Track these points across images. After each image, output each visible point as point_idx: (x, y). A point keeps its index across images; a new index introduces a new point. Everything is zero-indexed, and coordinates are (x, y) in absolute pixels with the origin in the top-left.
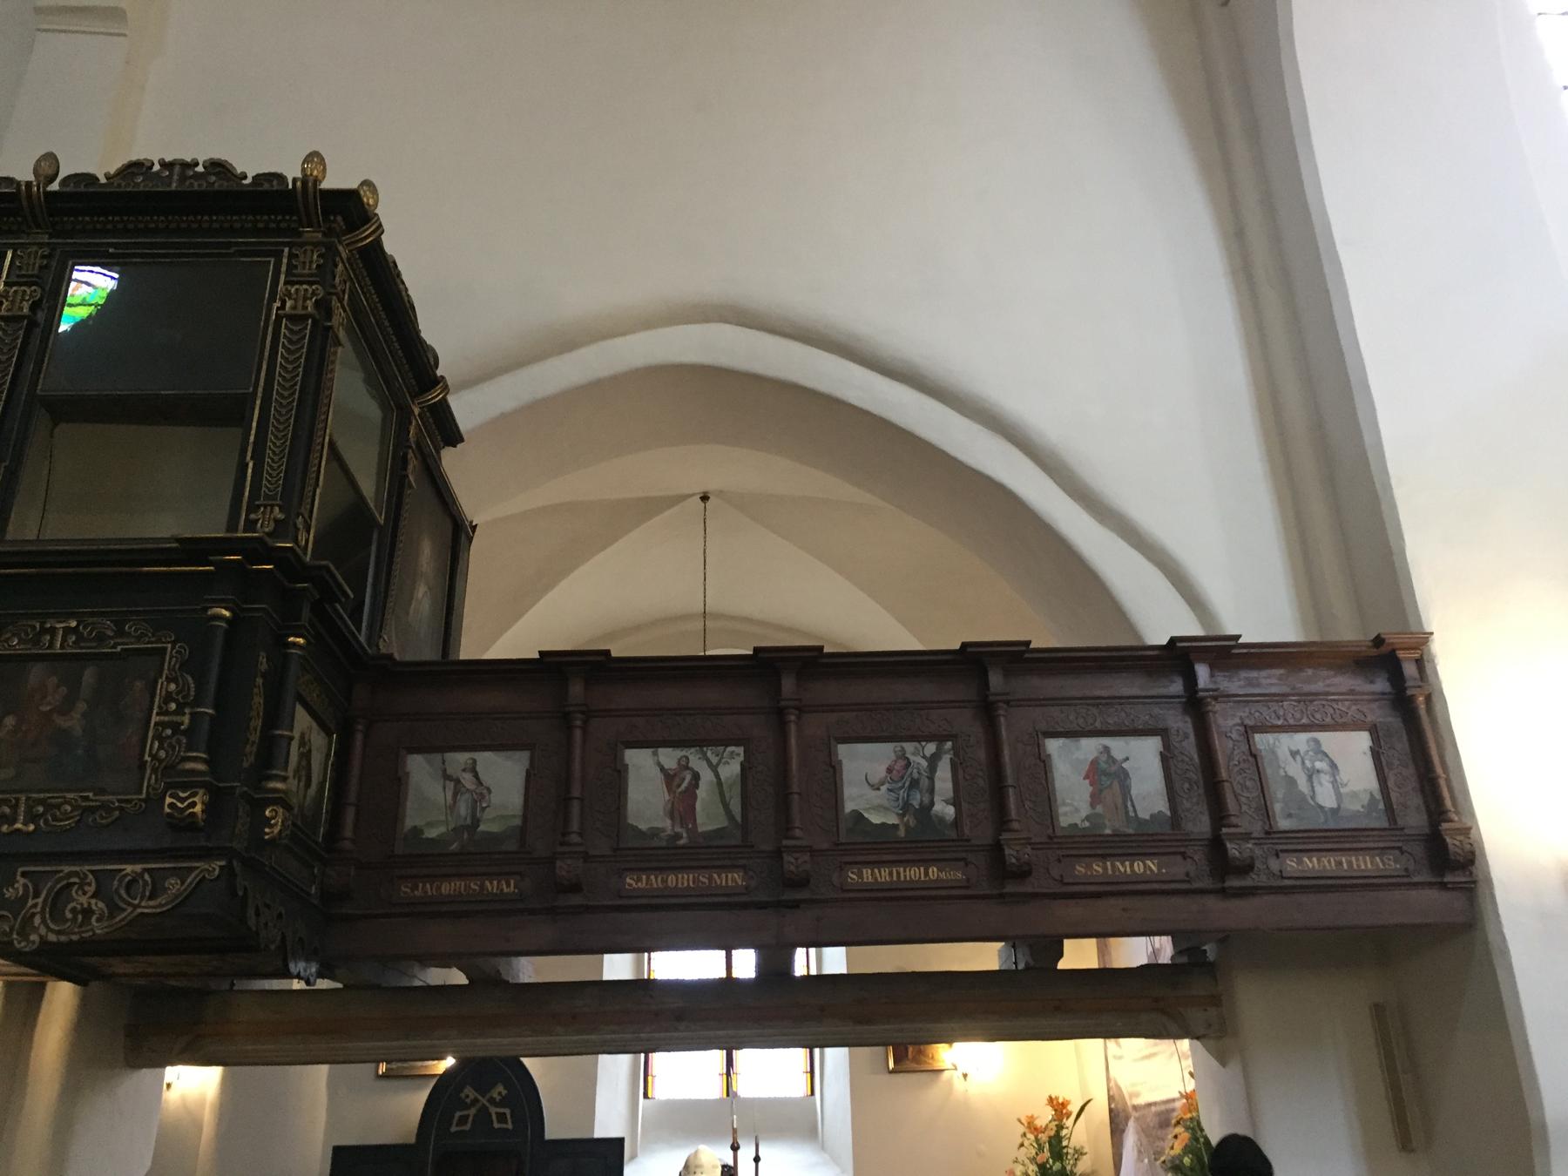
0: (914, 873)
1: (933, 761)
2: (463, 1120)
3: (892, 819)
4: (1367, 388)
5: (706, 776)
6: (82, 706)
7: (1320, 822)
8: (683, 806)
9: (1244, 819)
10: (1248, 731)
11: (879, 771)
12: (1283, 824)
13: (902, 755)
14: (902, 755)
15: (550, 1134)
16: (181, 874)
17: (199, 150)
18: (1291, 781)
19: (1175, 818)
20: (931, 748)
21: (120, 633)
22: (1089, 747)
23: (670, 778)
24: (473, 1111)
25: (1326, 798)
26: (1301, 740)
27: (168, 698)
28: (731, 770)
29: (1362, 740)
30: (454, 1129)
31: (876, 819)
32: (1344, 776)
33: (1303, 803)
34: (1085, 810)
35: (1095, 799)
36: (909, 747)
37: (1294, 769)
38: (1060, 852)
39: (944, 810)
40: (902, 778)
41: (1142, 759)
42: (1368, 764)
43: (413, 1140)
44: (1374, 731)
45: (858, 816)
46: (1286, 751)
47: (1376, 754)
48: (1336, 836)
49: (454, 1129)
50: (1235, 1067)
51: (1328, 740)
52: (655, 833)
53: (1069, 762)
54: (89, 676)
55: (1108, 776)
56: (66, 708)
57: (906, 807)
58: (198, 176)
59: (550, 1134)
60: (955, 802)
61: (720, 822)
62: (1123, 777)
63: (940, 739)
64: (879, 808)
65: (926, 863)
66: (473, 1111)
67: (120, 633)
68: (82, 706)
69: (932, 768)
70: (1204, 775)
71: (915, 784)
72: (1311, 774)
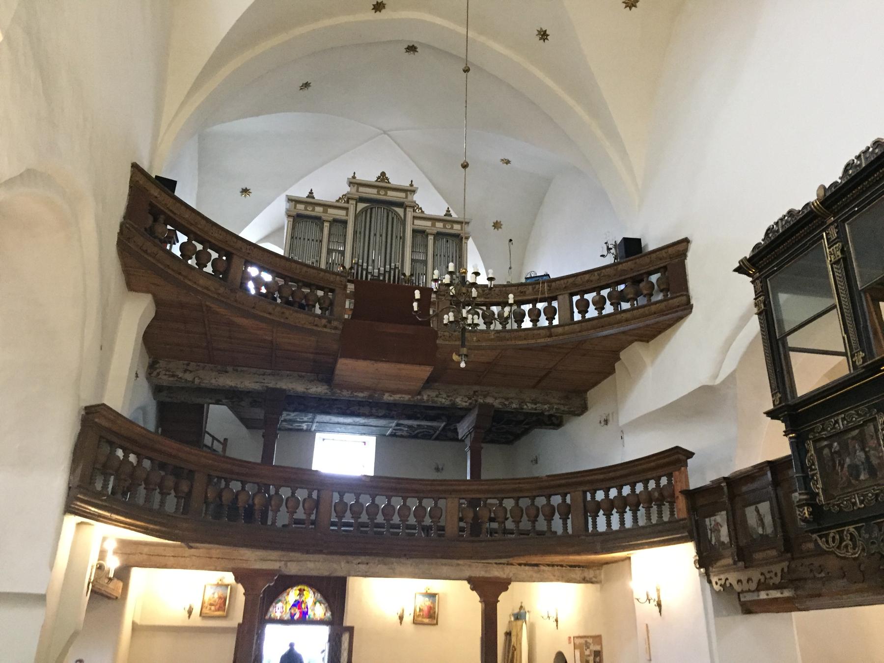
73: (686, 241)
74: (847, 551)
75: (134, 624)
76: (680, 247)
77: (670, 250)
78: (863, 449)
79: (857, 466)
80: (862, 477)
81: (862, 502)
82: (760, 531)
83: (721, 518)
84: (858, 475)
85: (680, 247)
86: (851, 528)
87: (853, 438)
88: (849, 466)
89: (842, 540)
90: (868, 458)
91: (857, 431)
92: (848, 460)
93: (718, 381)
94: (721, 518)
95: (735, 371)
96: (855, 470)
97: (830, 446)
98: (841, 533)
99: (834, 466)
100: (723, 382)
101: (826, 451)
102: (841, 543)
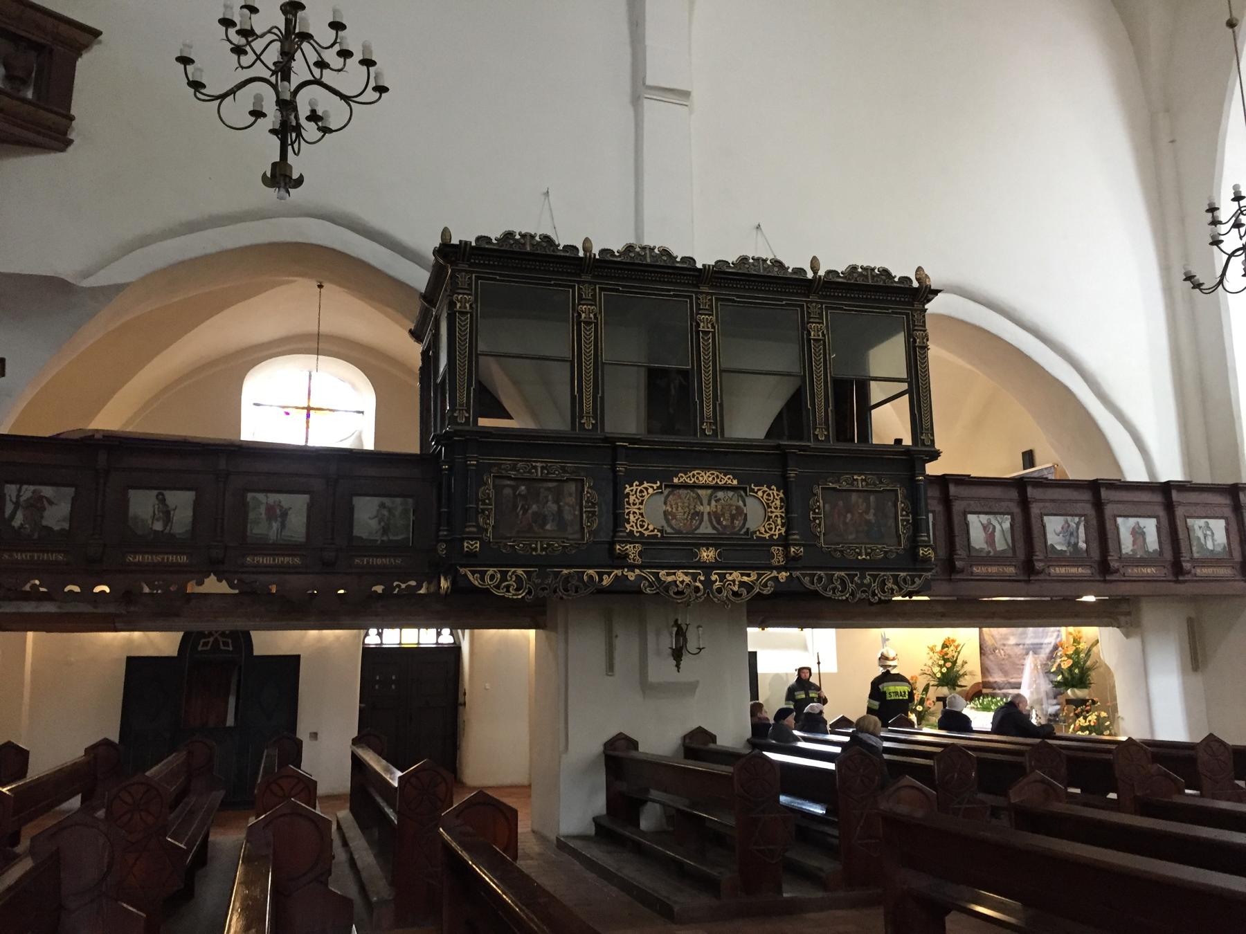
0: (1073, 570)
1: (1078, 524)
2: (205, 644)
3: (1064, 548)
4: (1235, 370)
5: (998, 527)
6: (872, 511)
7: (1209, 555)
8: (990, 539)
9: (1185, 555)
10: (1186, 517)
11: (1059, 529)
12: (1196, 555)
13: (1067, 522)
14: (1067, 522)
15: (256, 653)
16: (920, 577)
17: (877, 263)
18: (1199, 538)
19: (1161, 552)
20: (1077, 519)
21: (881, 482)
22: (1132, 522)
23: (985, 528)
24: (211, 639)
25: (1210, 546)
26: (1202, 522)
27: (903, 510)
28: (1007, 525)
29: (1222, 523)
30: (200, 648)
31: (1059, 548)
32: (1216, 537)
33: (1202, 547)
34: (1131, 547)
35: (1134, 543)
36: (1069, 518)
37: (1200, 534)
38: (467, 428)
39: (1083, 545)
40: (1069, 533)
41: (1150, 526)
42: (1224, 533)
43: (175, 654)
44: (1226, 519)
45: (1052, 546)
46: (1197, 524)
47: (1227, 530)
48: (1213, 560)
49: (200, 648)
50: (1135, 642)
51: (1212, 522)
52: (981, 550)
53: (1125, 526)
54: (872, 498)
55: (1138, 533)
56: (867, 512)
57: (1069, 544)
58: (873, 277)
59: (256, 653)
60: (1086, 542)
61: (1005, 547)
62: (1143, 534)
63: (1080, 516)
64: (1059, 543)
65: (1078, 566)
66: (211, 639)
67: (881, 482)
68: (872, 511)
69: (1078, 528)
70: (1173, 534)
71: (1072, 534)
72: (1205, 536)
73: (96, 34)
74: (508, 591)
75: (292, 662)
76: (83, 37)
77: (63, 28)
78: (557, 501)
79: (545, 517)
80: (548, 527)
81: (543, 549)
82: (158, 526)
83: (142, 504)
84: (545, 524)
85: (83, 37)
86: (520, 571)
87: (549, 489)
88: (534, 513)
89: (504, 579)
90: (560, 510)
91: (555, 484)
92: (535, 507)
93: (86, 283)
94: (142, 504)
95: (127, 284)
96: (541, 519)
97: (515, 488)
98: (504, 574)
99: (515, 507)
100: (92, 290)
101: (507, 491)
102: (501, 582)
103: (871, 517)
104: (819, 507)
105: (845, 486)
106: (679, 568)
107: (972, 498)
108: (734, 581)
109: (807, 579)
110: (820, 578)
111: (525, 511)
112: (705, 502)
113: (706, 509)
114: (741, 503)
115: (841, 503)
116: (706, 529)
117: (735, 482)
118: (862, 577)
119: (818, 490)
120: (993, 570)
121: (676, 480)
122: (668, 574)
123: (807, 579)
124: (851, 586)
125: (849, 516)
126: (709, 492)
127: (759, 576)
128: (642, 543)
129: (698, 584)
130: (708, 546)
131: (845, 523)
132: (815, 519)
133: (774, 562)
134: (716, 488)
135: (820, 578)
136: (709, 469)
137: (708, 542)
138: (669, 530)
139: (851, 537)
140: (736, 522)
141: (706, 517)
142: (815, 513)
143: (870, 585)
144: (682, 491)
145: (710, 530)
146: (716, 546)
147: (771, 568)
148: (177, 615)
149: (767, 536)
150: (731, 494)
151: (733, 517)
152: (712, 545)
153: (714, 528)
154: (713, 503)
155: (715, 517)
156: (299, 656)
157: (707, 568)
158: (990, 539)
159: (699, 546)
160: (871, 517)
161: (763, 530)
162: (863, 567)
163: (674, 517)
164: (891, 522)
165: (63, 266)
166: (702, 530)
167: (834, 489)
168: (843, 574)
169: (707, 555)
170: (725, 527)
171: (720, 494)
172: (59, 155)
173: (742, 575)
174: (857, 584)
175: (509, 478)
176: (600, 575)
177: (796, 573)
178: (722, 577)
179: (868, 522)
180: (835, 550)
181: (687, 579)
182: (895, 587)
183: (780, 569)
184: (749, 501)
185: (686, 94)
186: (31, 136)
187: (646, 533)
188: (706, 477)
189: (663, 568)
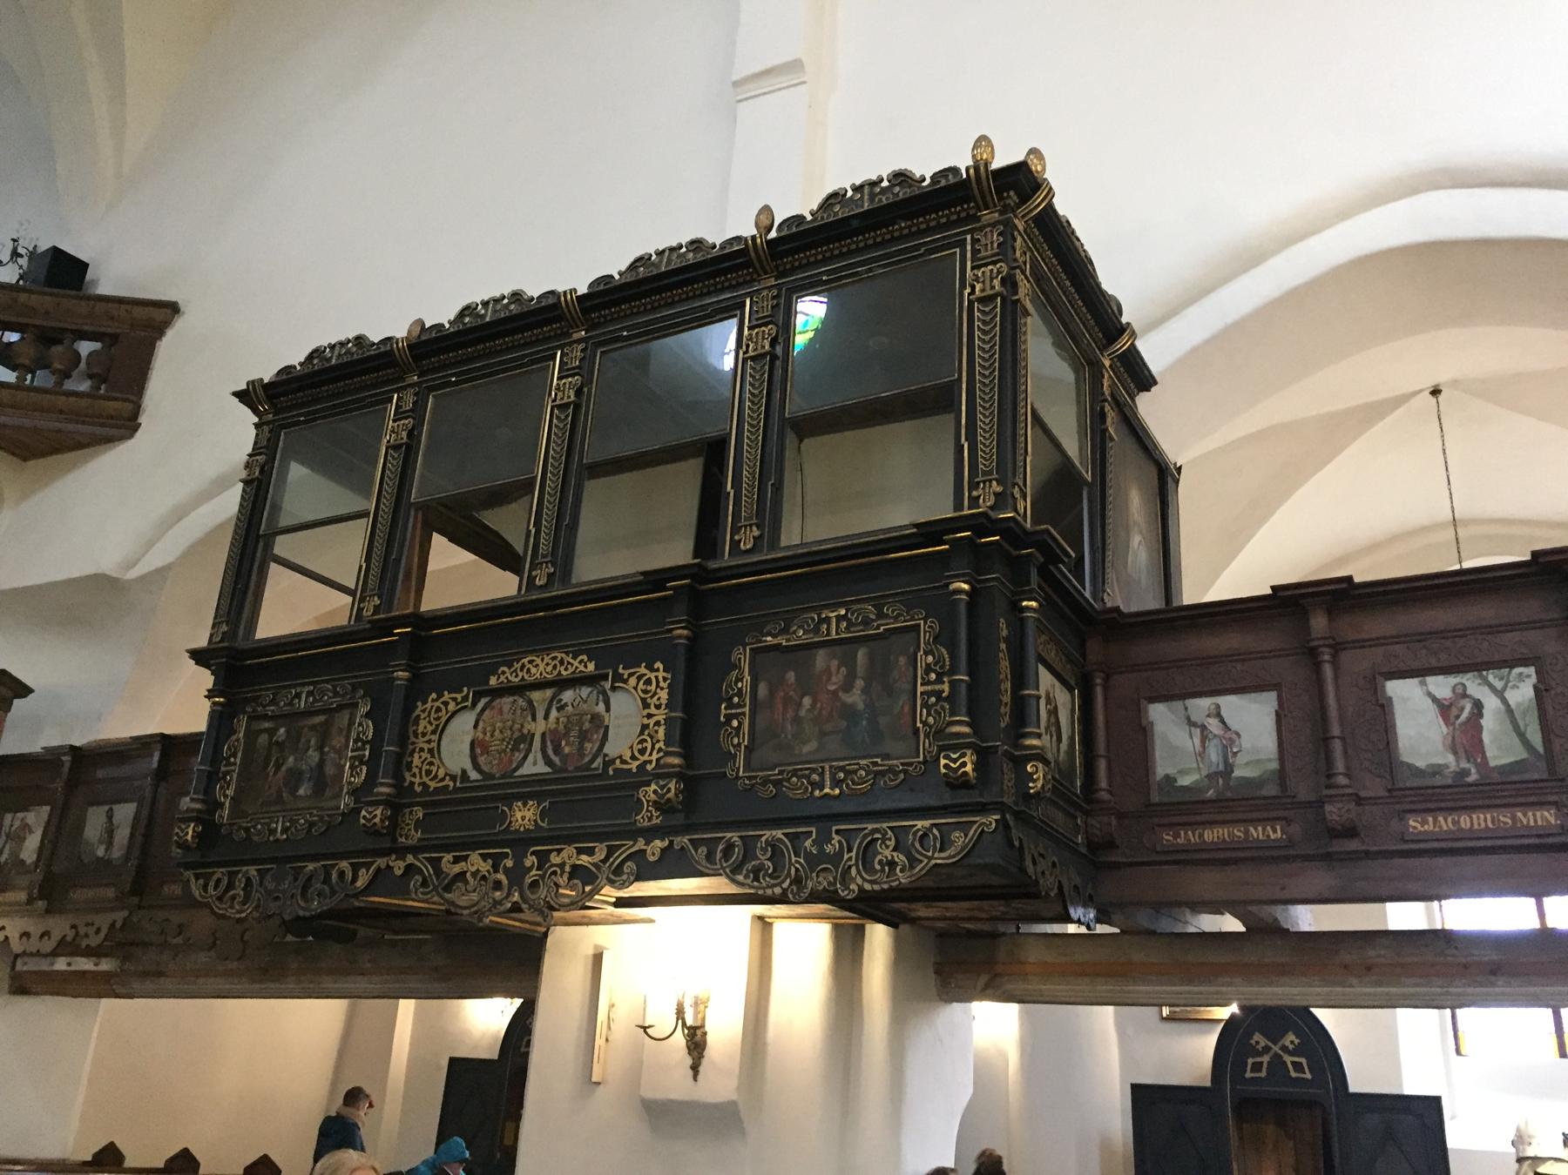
5: (1491, 703)
6: (860, 683)
8: (1467, 736)
17: (880, 168)
21: (881, 615)
23: (1445, 709)
27: (928, 669)
52: (1436, 770)
54: (861, 655)
56: (847, 686)
61: (1520, 754)
68: (860, 683)
76: (159, 315)
77: (138, 312)
78: (320, 748)
80: (301, 792)
82: (100, 852)
85: (159, 315)
88: (290, 770)
93: (132, 574)
97: (272, 732)
101: (263, 739)
103: (855, 698)
104: (740, 693)
105: (801, 635)
106: (474, 846)
107: (1397, 639)
108: (562, 866)
109: (703, 850)
110: (730, 847)
111: (278, 767)
112: (540, 714)
113: (539, 727)
114: (601, 707)
115: (791, 676)
116: (534, 766)
117: (591, 667)
118: (824, 838)
119: (743, 657)
120: (1478, 821)
121: (493, 681)
122: (456, 860)
123: (703, 850)
124: (796, 862)
125: (807, 701)
126: (549, 693)
127: (611, 850)
128: (423, 805)
129: (501, 876)
130: (524, 798)
131: (797, 720)
132: (729, 718)
133: (642, 820)
134: (561, 684)
135: (730, 847)
136: (548, 650)
137: (530, 790)
138: (474, 775)
139: (806, 749)
140: (588, 745)
141: (537, 739)
142: (730, 706)
143: (840, 854)
144: (507, 701)
145: (542, 768)
146: (538, 796)
147: (635, 833)
148: (160, 974)
149: (634, 765)
150: (585, 691)
151: (584, 737)
152: (531, 796)
153: (548, 762)
154: (554, 713)
155: (554, 739)
156: (1137, 1089)
157: (521, 842)
158: (1467, 736)
159: (509, 800)
160: (855, 698)
161: (627, 756)
162: (825, 819)
163: (486, 751)
164: (902, 702)
165: (107, 560)
166: (528, 769)
167: (777, 647)
168: (779, 834)
169: (524, 816)
170: (564, 758)
171: (567, 696)
172: (129, 443)
173: (580, 851)
174: (808, 856)
175: (265, 717)
176: (355, 868)
177: (682, 840)
178: (543, 858)
179: (849, 713)
180: (766, 781)
181: (485, 867)
182: (900, 858)
183: (650, 834)
184: (617, 699)
185: (795, 66)
186: (98, 430)
187: (433, 785)
188: (540, 667)
189: (447, 848)
